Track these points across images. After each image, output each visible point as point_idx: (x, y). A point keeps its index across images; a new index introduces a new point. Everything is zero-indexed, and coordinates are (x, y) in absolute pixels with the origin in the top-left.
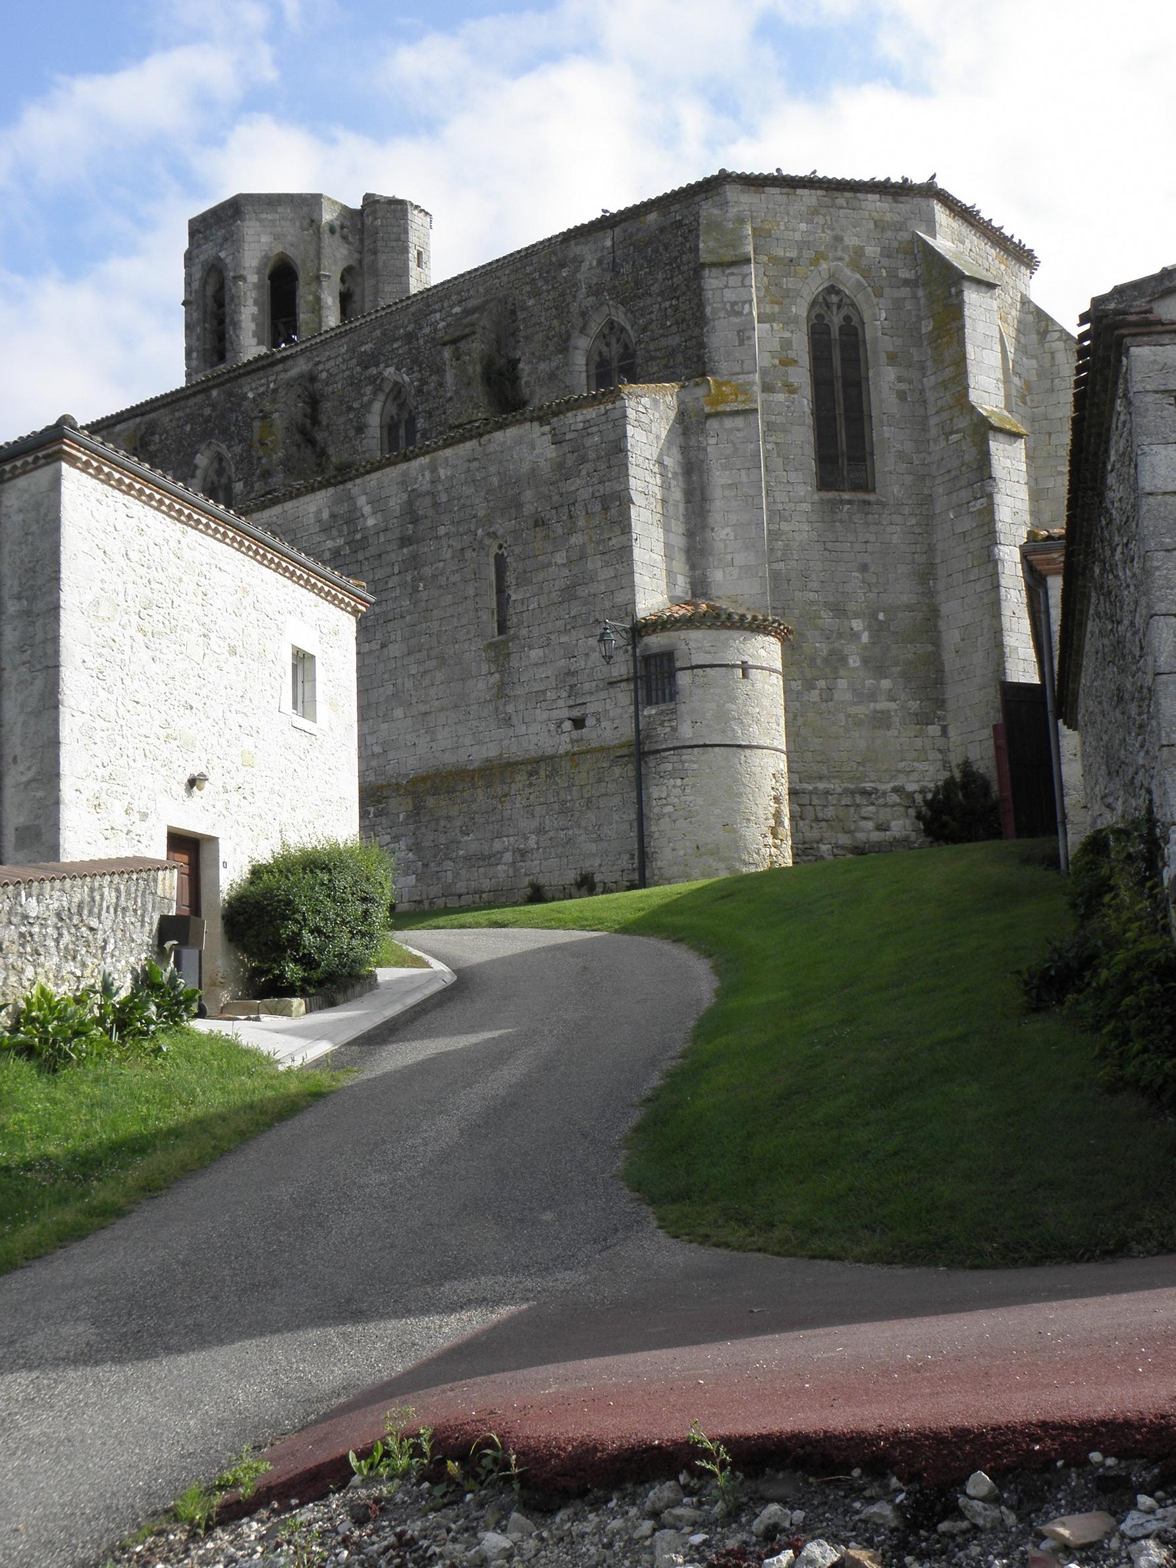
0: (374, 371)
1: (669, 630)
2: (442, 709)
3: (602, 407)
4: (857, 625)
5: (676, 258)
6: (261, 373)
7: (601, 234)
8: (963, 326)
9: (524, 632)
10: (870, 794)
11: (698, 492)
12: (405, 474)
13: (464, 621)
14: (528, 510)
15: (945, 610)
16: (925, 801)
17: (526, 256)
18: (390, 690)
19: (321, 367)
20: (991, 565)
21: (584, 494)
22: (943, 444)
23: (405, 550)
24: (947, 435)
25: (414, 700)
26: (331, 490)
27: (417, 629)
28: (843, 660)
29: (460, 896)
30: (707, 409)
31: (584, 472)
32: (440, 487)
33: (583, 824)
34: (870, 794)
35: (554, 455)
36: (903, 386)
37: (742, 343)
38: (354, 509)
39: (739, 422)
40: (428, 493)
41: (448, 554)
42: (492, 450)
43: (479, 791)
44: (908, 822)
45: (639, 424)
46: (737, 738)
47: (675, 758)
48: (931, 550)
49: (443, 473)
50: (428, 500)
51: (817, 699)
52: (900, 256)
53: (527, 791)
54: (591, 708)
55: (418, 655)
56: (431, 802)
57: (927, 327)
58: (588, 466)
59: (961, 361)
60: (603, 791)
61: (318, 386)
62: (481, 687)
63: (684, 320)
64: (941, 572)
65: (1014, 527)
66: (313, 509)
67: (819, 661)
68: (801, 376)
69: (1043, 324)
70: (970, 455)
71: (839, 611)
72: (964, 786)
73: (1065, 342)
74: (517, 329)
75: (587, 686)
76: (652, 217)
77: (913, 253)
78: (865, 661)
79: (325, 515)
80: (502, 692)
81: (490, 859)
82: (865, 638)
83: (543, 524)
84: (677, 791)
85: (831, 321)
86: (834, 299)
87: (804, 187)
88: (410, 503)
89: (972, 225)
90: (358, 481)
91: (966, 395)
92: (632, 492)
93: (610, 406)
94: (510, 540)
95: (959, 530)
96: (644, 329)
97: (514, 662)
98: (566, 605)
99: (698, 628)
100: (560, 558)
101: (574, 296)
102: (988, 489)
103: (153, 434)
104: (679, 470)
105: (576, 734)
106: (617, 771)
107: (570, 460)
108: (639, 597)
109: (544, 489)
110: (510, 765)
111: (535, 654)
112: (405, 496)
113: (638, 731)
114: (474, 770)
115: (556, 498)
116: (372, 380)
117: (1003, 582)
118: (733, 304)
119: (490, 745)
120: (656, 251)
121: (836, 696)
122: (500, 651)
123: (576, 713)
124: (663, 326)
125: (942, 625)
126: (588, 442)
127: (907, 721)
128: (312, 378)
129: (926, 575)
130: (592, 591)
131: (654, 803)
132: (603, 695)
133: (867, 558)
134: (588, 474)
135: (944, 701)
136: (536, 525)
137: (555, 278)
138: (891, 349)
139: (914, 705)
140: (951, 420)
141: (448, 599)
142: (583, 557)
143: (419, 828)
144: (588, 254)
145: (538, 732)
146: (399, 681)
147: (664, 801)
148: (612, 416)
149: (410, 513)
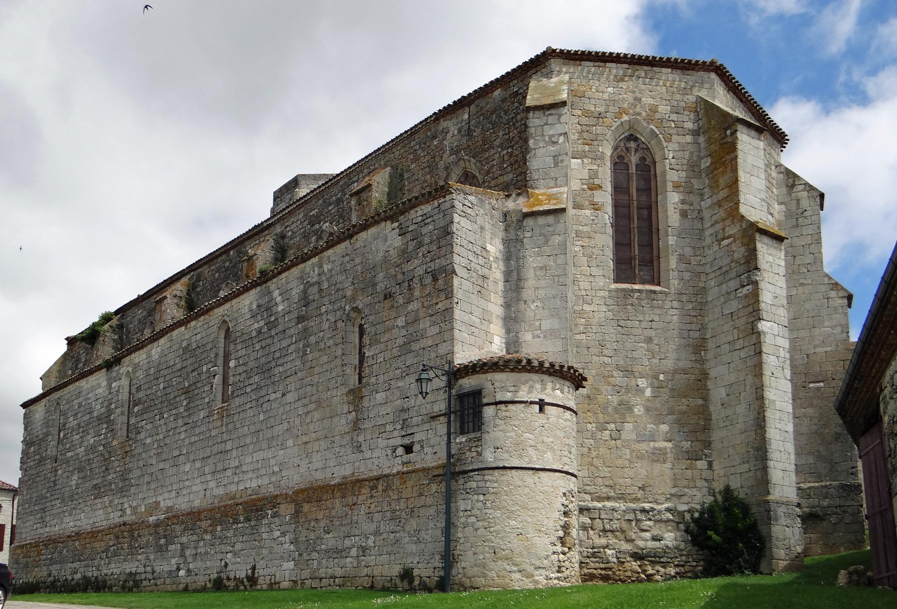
0: (317, 226)
1: (478, 373)
2: (318, 439)
3: (436, 202)
4: (642, 382)
5: (512, 118)
6: (256, 237)
7: (461, 111)
8: (736, 157)
9: (373, 380)
10: (648, 512)
11: (515, 274)
12: (303, 272)
13: (334, 374)
14: (380, 287)
15: (713, 373)
16: (692, 518)
17: (411, 135)
18: (285, 426)
19: (288, 229)
20: (754, 336)
21: (420, 271)
22: (716, 248)
23: (300, 326)
24: (719, 241)
25: (300, 433)
26: (259, 288)
27: (304, 381)
28: (630, 409)
29: (321, 579)
30: (525, 210)
31: (420, 254)
32: (324, 278)
33: (407, 529)
34: (648, 512)
35: (400, 243)
36: (686, 207)
37: (556, 164)
38: (272, 299)
39: (550, 219)
40: (316, 283)
41: (326, 326)
42: (358, 246)
43: (337, 500)
44: (679, 534)
45: (465, 215)
46: (531, 461)
47: (479, 478)
48: (703, 328)
49: (326, 267)
50: (315, 289)
51: (608, 438)
52: (686, 113)
53: (369, 501)
54: (417, 438)
55: (304, 401)
56: (306, 507)
57: (706, 163)
58: (424, 249)
59: (734, 185)
60: (422, 503)
61: (286, 240)
62: (342, 423)
63: (516, 162)
64: (711, 344)
65: (774, 308)
66: (247, 303)
67: (610, 409)
68: (605, 198)
69: (791, 180)
70: (740, 252)
71: (628, 372)
72: (727, 510)
73: (808, 191)
74: (404, 185)
75: (415, 420)
76: (497, 93)
77: (696, 111)
78: (648, 410)
79: (254, 306)
80: (356, 426)
81: (340, 553)
82: (648, 393)
83: (390, 296)
84: (480, 505)
85: (630, 161)
86: (632, 145)
87: (612, 61)
88: (305, 292)
89: (741, 101)
90: (274, 280)
91: (737, 208)
92: (455, 266)
93: (442, 200)
94: (367, 311)
95: (726, 312)
96: (488, 172)
97: (365, 403)
98: (403, 358)
99: (502, 371)
100: (400, 322)
101: (441, 157)
102: (754, 278)
103: (199, 281)
104: (500, 256)
105: (406, 458)
106: (434, 487)
107: (412, 246)
108: (457, 348)
109: (392, 271)
110: (359, 481)
111: (380, 397)
112: (302, 287)
113: (449, 456)
114: (335, 485)
115: (400, 276)
116: (316, 232)
117: (764, 349)
118: (551, 136)
119: (347, 466)
120: (499, 116)
121: (623, 437)
122: (356, 396)
123: (407, 441)
124: (501, 168)
125: (710, 384)
126: (425, 230)
127: (680, 457)
128: (283, 237)
129: (698, 347)
130: (422, 346)
131: (462, 514)
132: (426, 426)
133: (652, 333)
134: (423, 255)
135: (710, 443)
136: (385, 298)
137: (429, 146)
138: (676, 179)
139: (686, 445)
140: (724, 229)
141: (325, 359)
142: (416, 320)
143: (297, 527)
144: (451, 126)
145: (380, 458)
146: (292, 420)
147: (469, 513)
148: (443, 208)
149: (305, 300)
